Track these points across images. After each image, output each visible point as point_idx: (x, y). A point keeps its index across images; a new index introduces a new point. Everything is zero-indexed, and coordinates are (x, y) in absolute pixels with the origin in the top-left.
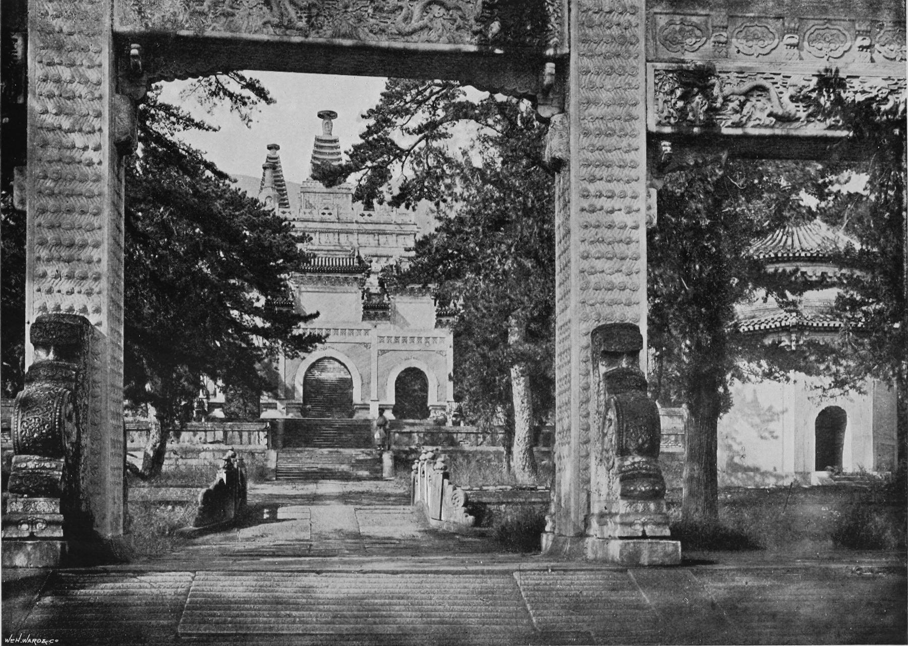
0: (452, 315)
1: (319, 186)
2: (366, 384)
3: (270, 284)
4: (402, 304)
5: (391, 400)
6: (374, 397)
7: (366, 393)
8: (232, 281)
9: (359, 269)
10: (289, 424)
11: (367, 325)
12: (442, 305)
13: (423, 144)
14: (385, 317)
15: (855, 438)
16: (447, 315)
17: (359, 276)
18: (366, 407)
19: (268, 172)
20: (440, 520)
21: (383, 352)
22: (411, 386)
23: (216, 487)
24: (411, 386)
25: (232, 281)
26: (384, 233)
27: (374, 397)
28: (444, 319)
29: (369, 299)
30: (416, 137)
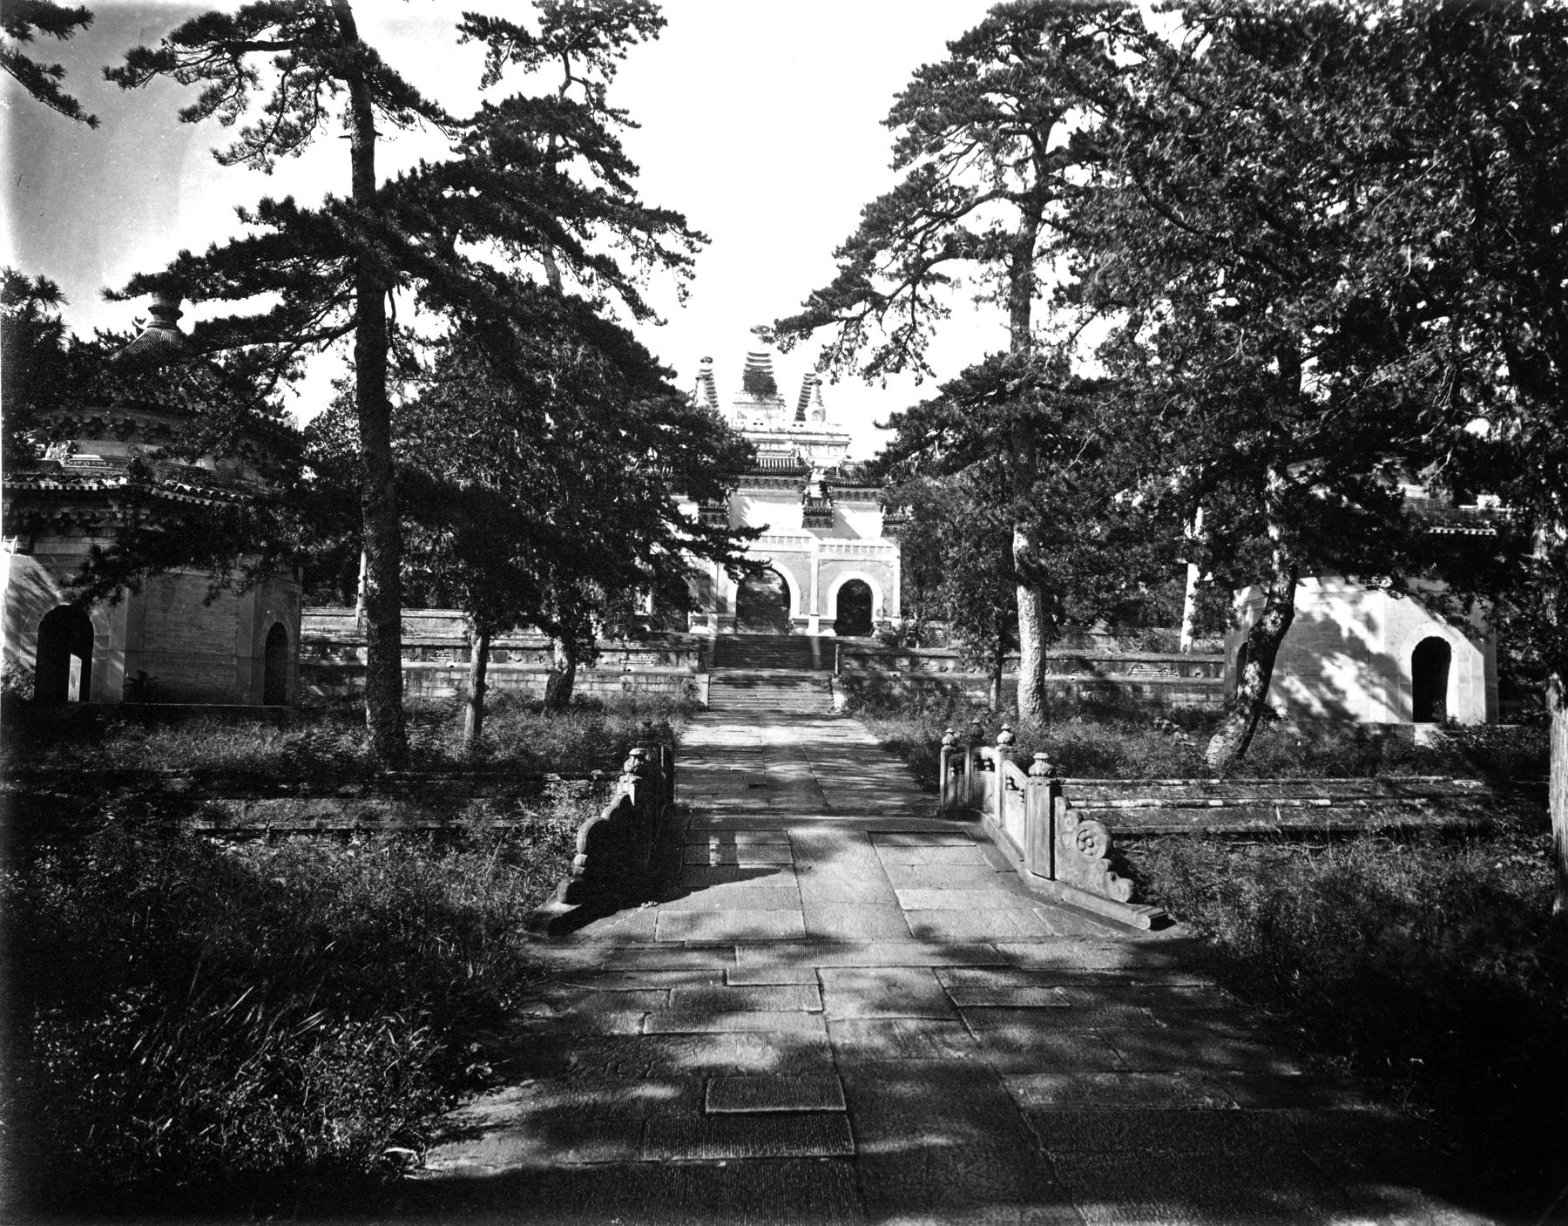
0: (901, 522)
1: (749, 398)
2: (805, 598)
3: (705, 487)
4: (844, 509)
5: (832, 614)
6: (813, 614)
7: (805, 608)
8: (663, 427)
9: (801, 472)
10: (722, 640)
11: (806, 532)
12: (889, 512)
13: (909, 288)
14: (829, 524)
15: (1462, 679)
16: (895, 523)
17: (799, 479)
18: (805, 624)
19: (702, 384)
20: (1052, 878)
21: (825, 562)
22: (854, 600)
23: (614, 813)
24: (854, 600)
25: (663, 427)
26: (816, 444)
27: (813, 614)
28: (891, 527)
29: (810, 504)
30: (898, 283)
